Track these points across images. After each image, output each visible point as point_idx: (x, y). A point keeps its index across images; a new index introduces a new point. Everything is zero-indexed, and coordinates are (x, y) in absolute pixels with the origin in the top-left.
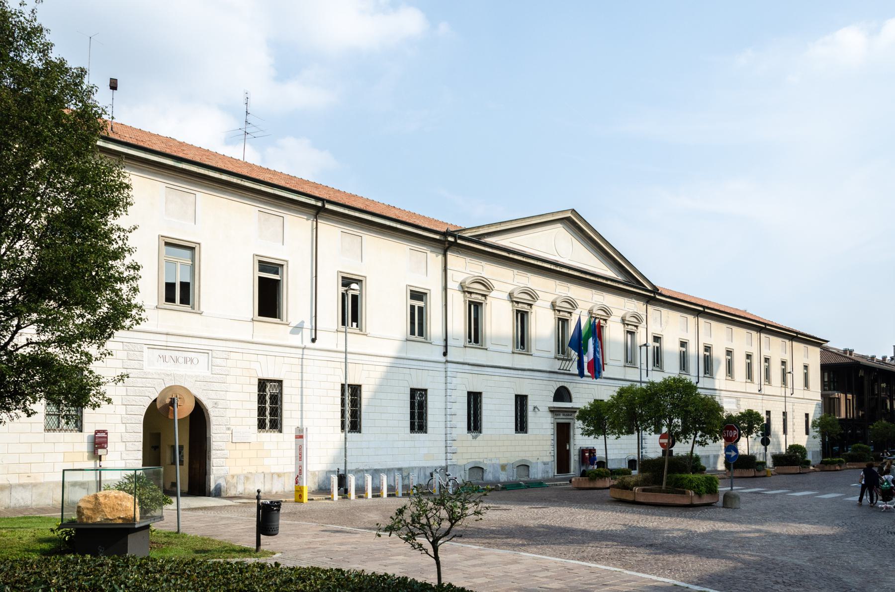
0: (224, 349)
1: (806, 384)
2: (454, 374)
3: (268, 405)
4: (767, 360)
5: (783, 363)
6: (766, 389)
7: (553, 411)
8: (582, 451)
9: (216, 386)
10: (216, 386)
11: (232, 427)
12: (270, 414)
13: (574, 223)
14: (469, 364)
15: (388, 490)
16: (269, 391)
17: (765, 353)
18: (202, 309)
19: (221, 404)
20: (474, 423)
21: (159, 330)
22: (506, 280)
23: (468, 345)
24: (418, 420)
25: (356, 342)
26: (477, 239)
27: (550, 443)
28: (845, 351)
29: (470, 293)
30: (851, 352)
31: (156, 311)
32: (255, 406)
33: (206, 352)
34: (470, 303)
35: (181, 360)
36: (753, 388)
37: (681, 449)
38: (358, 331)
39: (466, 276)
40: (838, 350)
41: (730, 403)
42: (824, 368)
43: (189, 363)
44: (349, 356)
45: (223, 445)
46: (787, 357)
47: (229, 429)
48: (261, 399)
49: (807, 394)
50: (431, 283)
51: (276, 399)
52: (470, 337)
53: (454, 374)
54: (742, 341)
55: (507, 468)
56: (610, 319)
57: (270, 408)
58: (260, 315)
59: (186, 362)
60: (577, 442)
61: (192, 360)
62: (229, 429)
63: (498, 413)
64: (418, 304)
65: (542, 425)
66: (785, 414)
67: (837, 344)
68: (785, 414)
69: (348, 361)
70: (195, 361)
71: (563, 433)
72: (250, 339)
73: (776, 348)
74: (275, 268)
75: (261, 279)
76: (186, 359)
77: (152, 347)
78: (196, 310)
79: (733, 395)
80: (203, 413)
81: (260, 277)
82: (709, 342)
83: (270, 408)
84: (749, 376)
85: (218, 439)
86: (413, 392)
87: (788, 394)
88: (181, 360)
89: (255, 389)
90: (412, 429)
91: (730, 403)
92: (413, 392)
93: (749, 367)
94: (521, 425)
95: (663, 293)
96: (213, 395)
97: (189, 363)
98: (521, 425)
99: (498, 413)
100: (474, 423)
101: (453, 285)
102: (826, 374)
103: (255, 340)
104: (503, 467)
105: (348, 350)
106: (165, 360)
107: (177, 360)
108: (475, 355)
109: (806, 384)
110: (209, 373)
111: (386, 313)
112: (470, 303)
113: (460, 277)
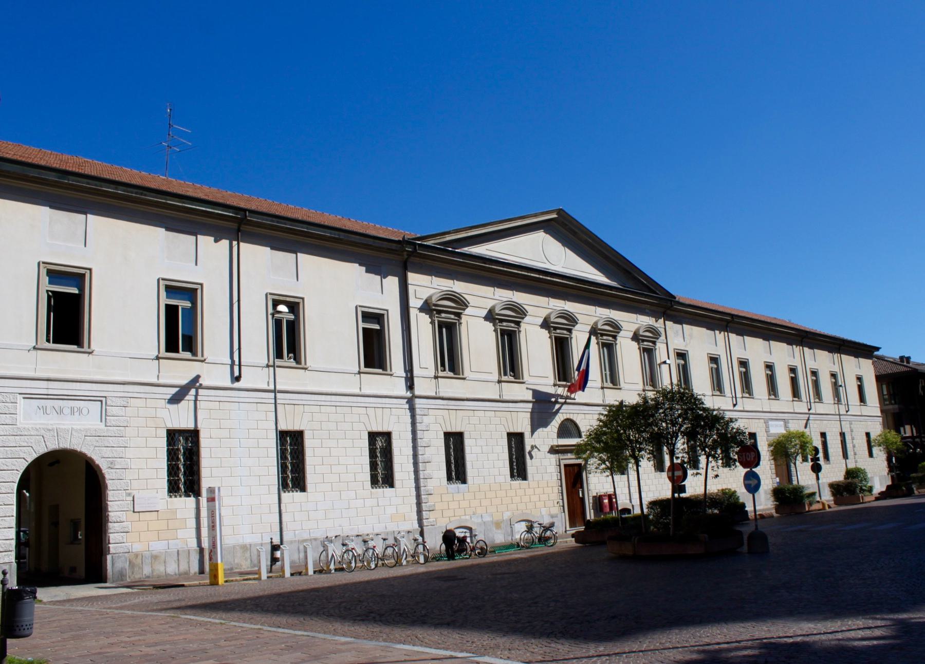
0: (316, 403)
1: (862, 399)
2: (426, 412)
3: (379, 460)
4: (814, 373)
5: (834, 375)
6: (818, 408)
7: (554, 450)
8: (598, 500)
9: (112, 441)
10: (112, 441)
11: (134, 492)
12: (292, 471)
13: (566, 230)
14: (443, 399)
15: (226, 575)
16: (380, 443)
17: (811, 365)
18: (93, 347)
19: (119, 463)
20: (457, 470)
21: (38, 375)
22: (482, 298)
23: (441, 374)
24: (382, 472)
25: (289, 378)
26: (442, 249)
27: (556, 490)
28: (902, 358)
29: (439, 312)
30: (908, 359)
31: (34, 352)
32: (367, 460)
33: (101, 400)
34: (503, 332)
35: (67, 411)
36: (801, 407)
37: (694, 486)
38: (292, 363)
39: (432, 291)
40: (895, 359)
41: (777, 426)
42: (879, 379)
43: (77, 414)
44: (278, 395)
45: (123, 516)
46: (836, 369)
47: (129, 494)
48: (172, 455)
49: (865, 411)
50: (720, 351)
51: (193, 455)
52: (443, 365)
53: (426, 412)
54: (783, 355)
55: (502, 525)
56: (620, 334)
57: (184, 463)
58: (366, 366)
59: (72, 412)
60: (591, 487)
61: (80, 411)
62: (129, 494)
63: (487, 457)
64: (183, 304)
65: (545, 469)
66: (843, 435)
67: (891, 350)
68: (843, 435)
69: (278, 401)
70: (85, 411)
71: (574, 478)
72: (154, 380)
73: (823, 361)
74: (78, 278)
75: (365, 330)
76: (72, 409)
77: (29, 397)
78: (303, 365)
79: (762, 417)
80: (97, 476)
81: (364, 329)
82: (744, 355)
83: (184, 463)
84: (796, 393)
85: (116, 508)
86: (373, 436)
87: (843, 412)
88: (67, 411)
89: (163, 442)
90: (374, 482)
91: (777, 426)
92: (373, 436)
93: (794, 382)
94: (519, 470)
95: (681, 301)
96: (107, 452)
97: (77, 414)
98: (519, 470)
99: (487, 457)
100: (457, 470)
101: (415, 303)
102: (884, 387)
103: (161, 381)
104: (498, 525)
105: (278, 388)
106: (45, 412)
107: (61, 411)
108: (450, 387)
109: (862, 399)
110: (102, 426)
111: (332, 338)
112: (441, 325)
113: (425, 294)
